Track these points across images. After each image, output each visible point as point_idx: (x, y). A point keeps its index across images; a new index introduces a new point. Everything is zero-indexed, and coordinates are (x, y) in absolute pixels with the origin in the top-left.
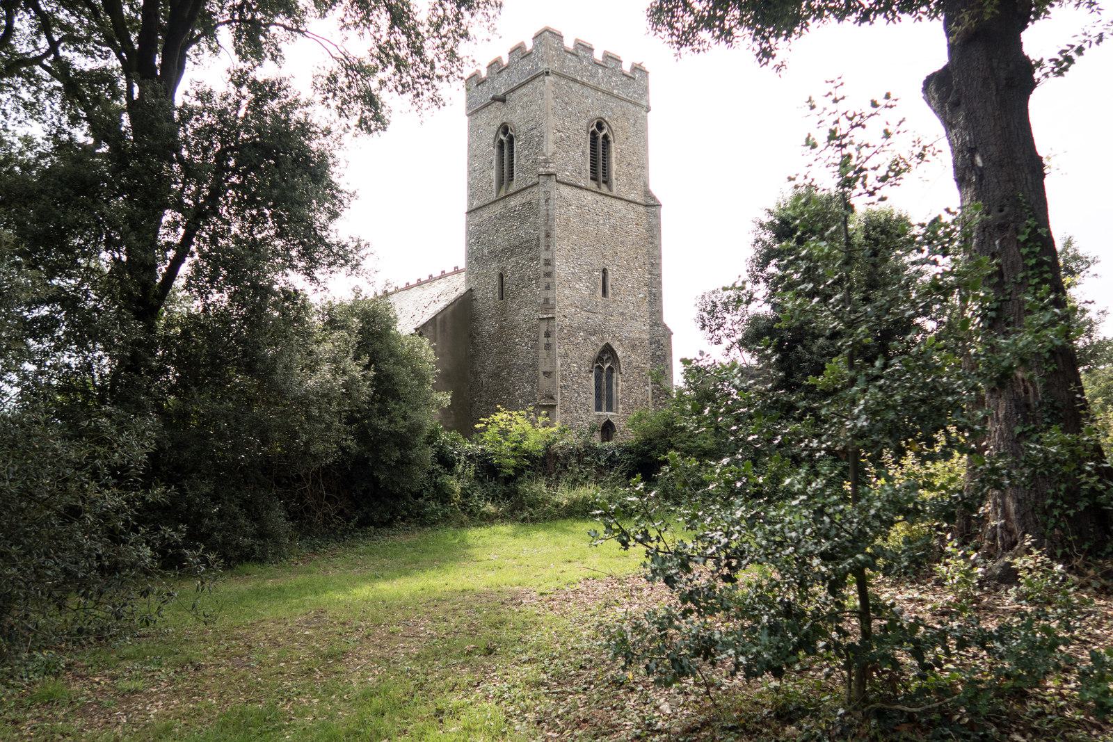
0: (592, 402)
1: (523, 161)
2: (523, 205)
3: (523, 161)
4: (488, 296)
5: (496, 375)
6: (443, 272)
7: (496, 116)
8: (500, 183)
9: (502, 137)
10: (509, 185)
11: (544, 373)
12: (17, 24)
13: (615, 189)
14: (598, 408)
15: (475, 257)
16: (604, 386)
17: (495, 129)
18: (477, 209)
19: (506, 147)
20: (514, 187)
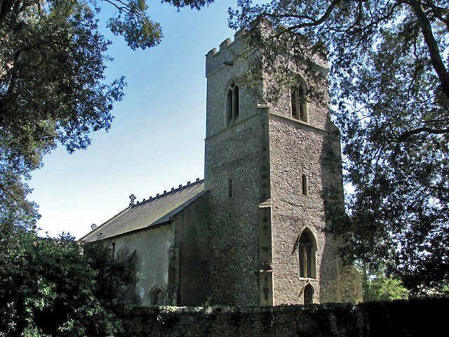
0: (297, 270)
1: (245, 101)
2: (245, 131)
3: (245, 101)
4: (221, 194)
5: (225, 251)
6: (189, 183)
7: (226, 76)
8: (230, 118)
9: (230, 88)
10: (235, 119)
11: (263, 248)
12: (227, 131)
13: (308, 120)
14: (302, 275)
15: (210, 167)
16: (298, 106)
17: (225, 83)
18: (214, 136)
19: (233, 94)
20: (240, 119)
